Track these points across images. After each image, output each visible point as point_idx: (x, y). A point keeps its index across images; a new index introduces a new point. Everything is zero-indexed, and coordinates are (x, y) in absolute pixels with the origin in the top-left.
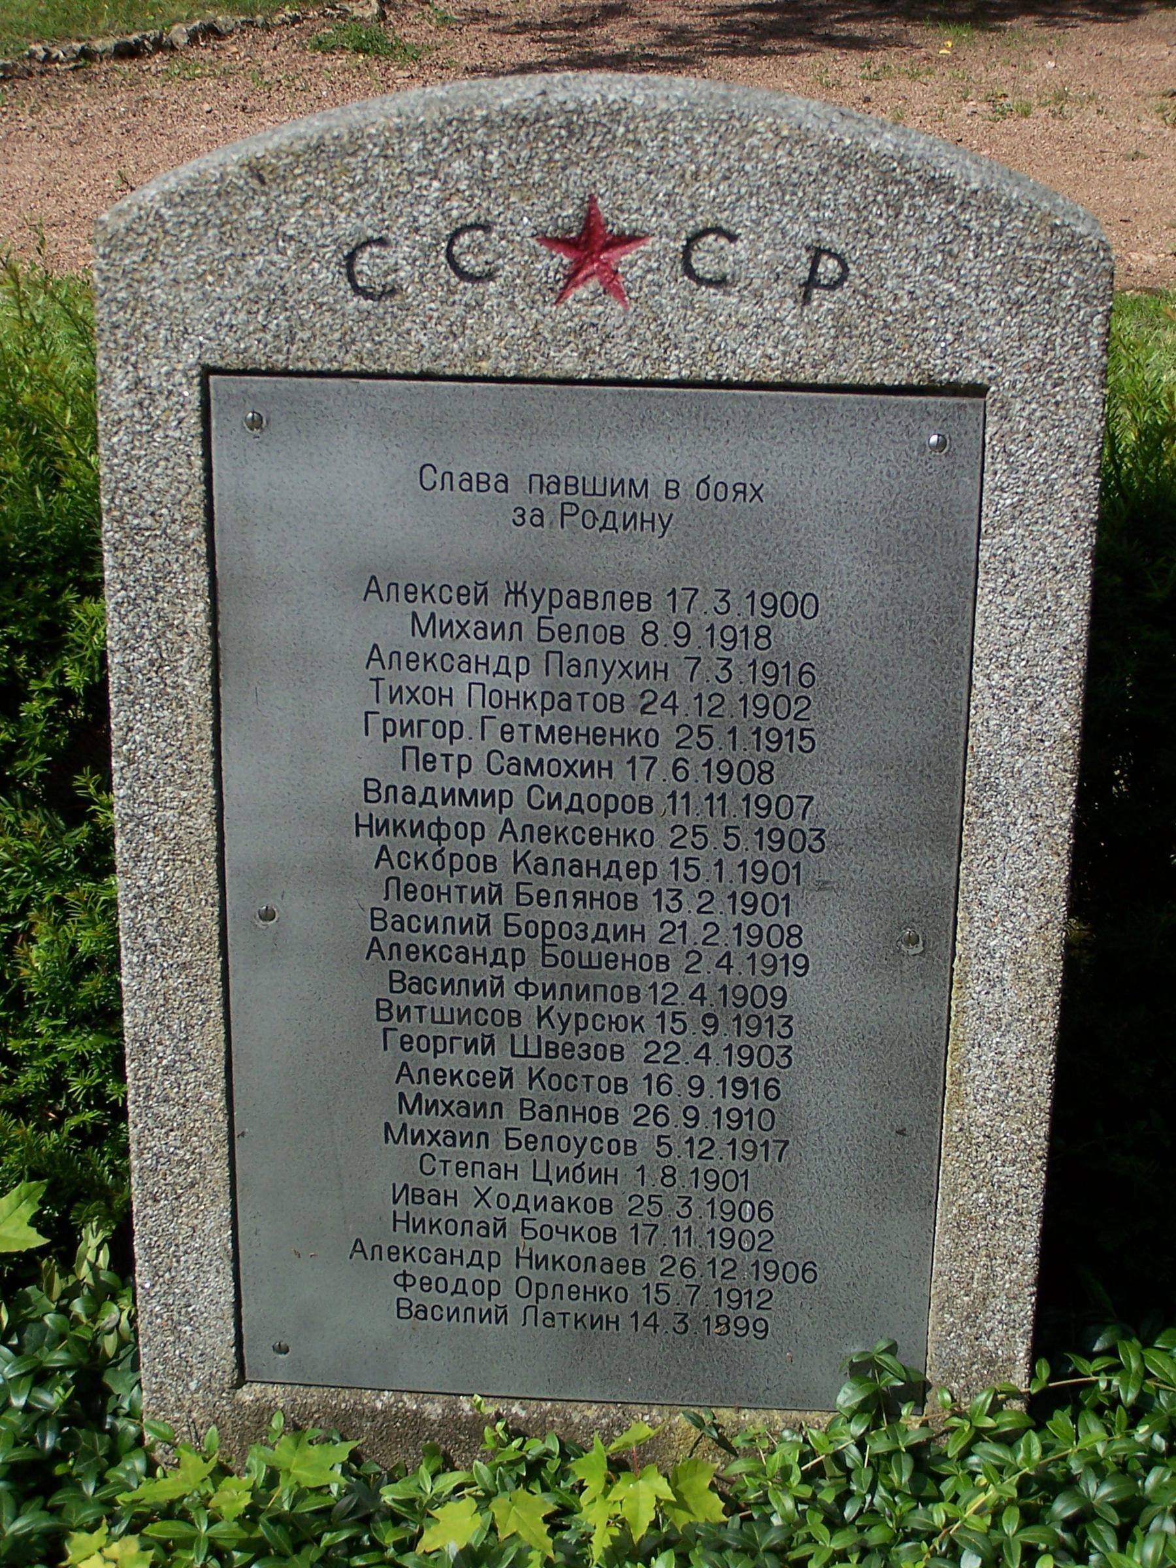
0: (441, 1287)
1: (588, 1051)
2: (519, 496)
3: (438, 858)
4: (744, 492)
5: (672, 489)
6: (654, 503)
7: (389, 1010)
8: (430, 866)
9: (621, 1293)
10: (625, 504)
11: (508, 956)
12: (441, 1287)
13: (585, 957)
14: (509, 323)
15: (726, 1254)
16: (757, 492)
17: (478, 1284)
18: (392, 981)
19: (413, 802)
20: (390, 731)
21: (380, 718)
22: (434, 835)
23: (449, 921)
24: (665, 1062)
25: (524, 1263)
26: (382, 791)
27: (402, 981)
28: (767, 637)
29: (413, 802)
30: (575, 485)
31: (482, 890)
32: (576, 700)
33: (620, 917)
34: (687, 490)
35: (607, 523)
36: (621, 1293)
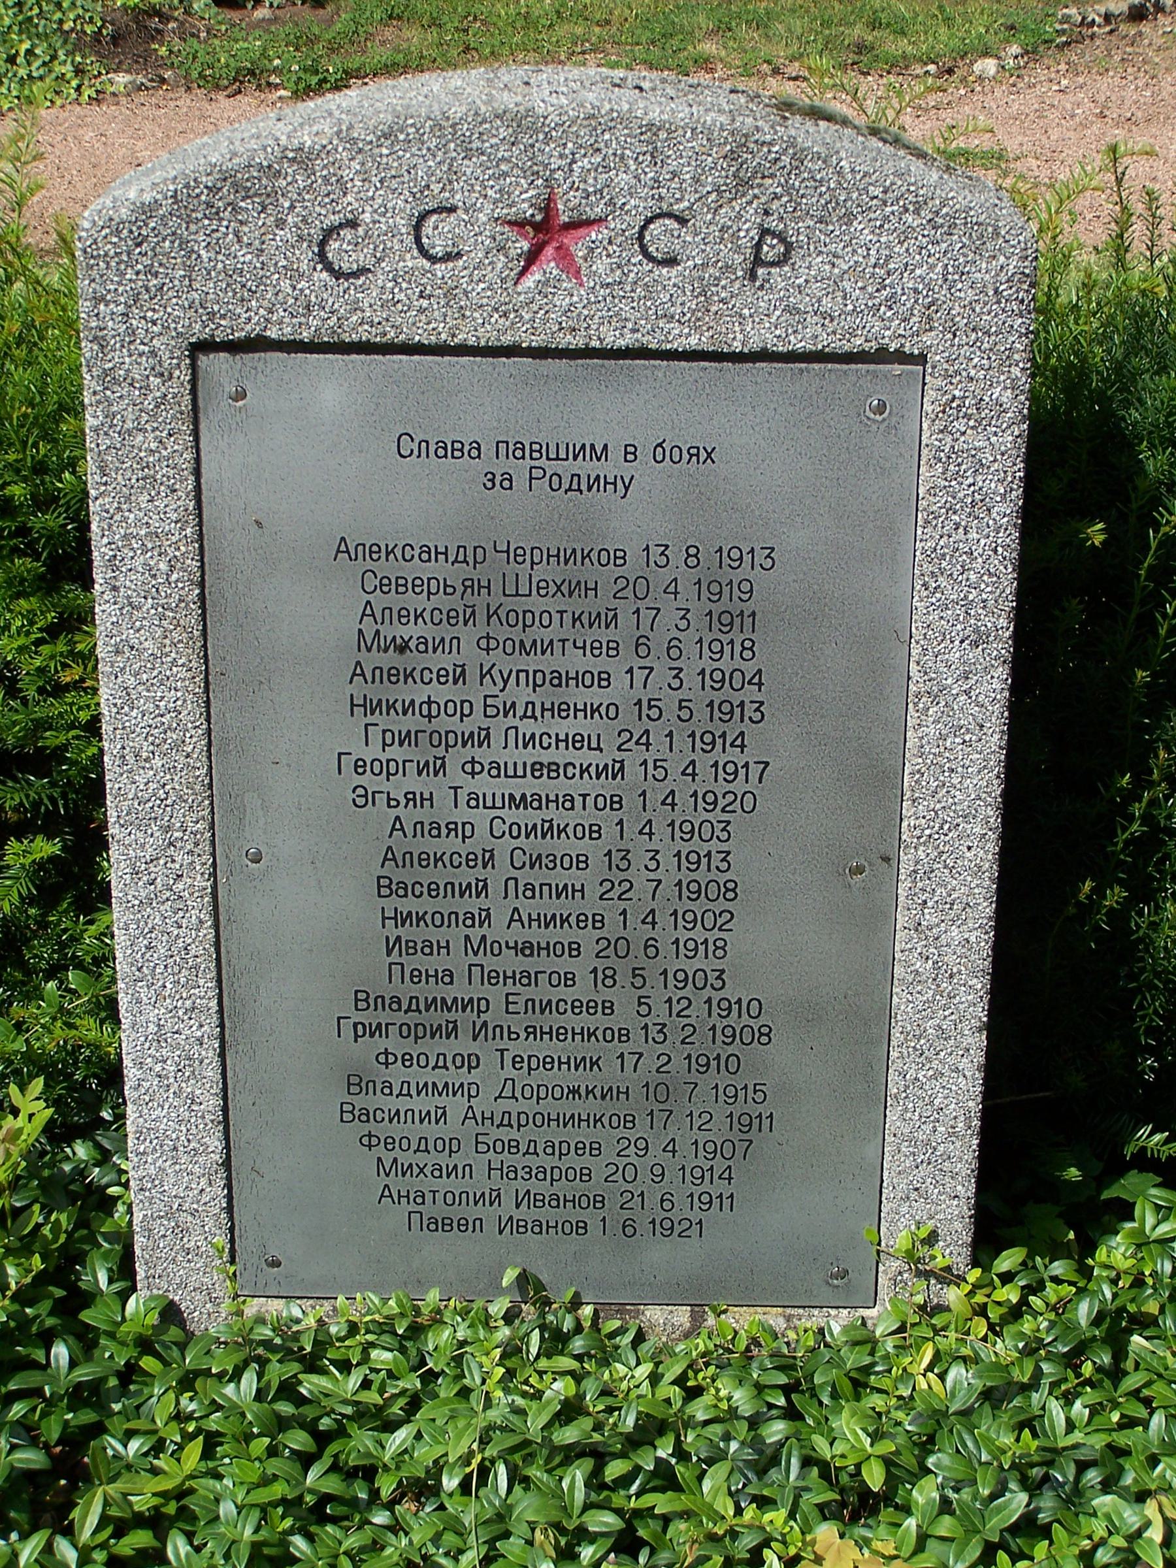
0: (405, 1146)
1: (554, 861)
2: (490, 462)
3: (659, 449)
4: (698, 455)
5: (630, 453)
6: (608, 469)
7: (366, 1000)
8: (448, 864)
9: (612, 709)
10: (587, 468)
11: (470, 552)
12: (405, 1146)
13: (553, 449)
14: (490, 295)
15: (681, 994)
16: (709, 455)
17: (439, 1142)
18: (379, 886)
19: (400, 1009)
20: (389, 741)
21: (380, 729)
22: (425, 712)
23: (387, 612)
24: (619, 898)
25: (495, 1174)
26: (363, 1085)
27: (389, 887)
28: (768, 1035)
29: (400, 1009)
30: (540, 451)
31: (469, 885)
32: (579, 801)
33: (595, 696)
34: (645, 454)
35: (575, 485)
36: (612, 709)
